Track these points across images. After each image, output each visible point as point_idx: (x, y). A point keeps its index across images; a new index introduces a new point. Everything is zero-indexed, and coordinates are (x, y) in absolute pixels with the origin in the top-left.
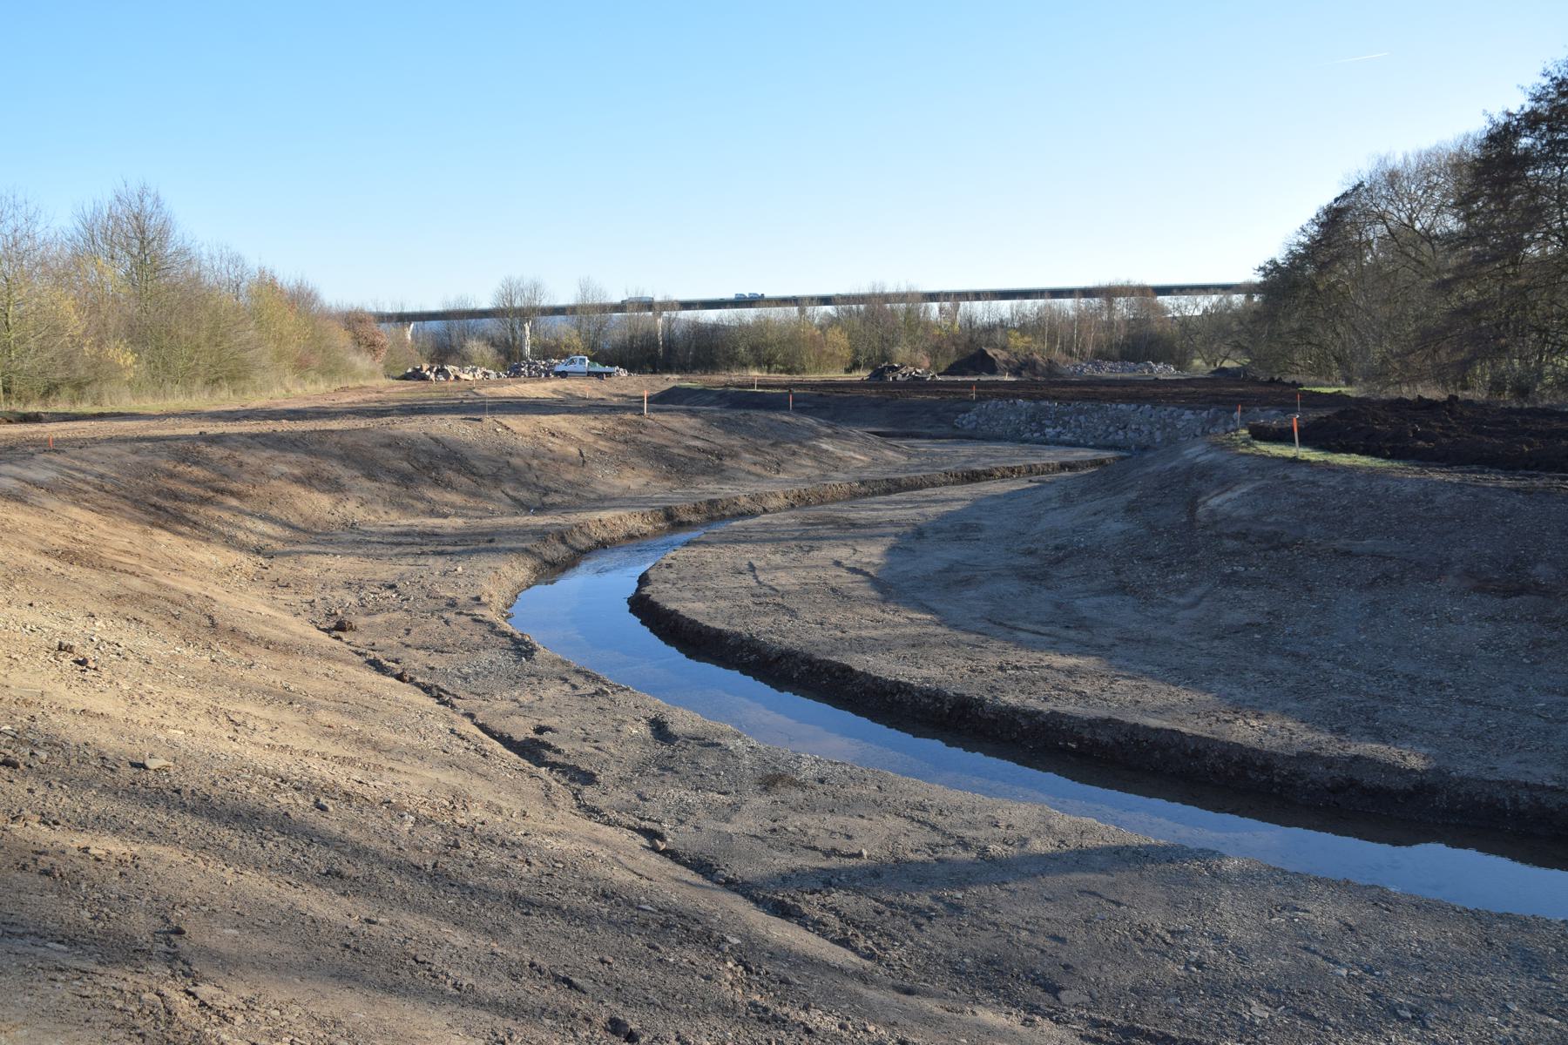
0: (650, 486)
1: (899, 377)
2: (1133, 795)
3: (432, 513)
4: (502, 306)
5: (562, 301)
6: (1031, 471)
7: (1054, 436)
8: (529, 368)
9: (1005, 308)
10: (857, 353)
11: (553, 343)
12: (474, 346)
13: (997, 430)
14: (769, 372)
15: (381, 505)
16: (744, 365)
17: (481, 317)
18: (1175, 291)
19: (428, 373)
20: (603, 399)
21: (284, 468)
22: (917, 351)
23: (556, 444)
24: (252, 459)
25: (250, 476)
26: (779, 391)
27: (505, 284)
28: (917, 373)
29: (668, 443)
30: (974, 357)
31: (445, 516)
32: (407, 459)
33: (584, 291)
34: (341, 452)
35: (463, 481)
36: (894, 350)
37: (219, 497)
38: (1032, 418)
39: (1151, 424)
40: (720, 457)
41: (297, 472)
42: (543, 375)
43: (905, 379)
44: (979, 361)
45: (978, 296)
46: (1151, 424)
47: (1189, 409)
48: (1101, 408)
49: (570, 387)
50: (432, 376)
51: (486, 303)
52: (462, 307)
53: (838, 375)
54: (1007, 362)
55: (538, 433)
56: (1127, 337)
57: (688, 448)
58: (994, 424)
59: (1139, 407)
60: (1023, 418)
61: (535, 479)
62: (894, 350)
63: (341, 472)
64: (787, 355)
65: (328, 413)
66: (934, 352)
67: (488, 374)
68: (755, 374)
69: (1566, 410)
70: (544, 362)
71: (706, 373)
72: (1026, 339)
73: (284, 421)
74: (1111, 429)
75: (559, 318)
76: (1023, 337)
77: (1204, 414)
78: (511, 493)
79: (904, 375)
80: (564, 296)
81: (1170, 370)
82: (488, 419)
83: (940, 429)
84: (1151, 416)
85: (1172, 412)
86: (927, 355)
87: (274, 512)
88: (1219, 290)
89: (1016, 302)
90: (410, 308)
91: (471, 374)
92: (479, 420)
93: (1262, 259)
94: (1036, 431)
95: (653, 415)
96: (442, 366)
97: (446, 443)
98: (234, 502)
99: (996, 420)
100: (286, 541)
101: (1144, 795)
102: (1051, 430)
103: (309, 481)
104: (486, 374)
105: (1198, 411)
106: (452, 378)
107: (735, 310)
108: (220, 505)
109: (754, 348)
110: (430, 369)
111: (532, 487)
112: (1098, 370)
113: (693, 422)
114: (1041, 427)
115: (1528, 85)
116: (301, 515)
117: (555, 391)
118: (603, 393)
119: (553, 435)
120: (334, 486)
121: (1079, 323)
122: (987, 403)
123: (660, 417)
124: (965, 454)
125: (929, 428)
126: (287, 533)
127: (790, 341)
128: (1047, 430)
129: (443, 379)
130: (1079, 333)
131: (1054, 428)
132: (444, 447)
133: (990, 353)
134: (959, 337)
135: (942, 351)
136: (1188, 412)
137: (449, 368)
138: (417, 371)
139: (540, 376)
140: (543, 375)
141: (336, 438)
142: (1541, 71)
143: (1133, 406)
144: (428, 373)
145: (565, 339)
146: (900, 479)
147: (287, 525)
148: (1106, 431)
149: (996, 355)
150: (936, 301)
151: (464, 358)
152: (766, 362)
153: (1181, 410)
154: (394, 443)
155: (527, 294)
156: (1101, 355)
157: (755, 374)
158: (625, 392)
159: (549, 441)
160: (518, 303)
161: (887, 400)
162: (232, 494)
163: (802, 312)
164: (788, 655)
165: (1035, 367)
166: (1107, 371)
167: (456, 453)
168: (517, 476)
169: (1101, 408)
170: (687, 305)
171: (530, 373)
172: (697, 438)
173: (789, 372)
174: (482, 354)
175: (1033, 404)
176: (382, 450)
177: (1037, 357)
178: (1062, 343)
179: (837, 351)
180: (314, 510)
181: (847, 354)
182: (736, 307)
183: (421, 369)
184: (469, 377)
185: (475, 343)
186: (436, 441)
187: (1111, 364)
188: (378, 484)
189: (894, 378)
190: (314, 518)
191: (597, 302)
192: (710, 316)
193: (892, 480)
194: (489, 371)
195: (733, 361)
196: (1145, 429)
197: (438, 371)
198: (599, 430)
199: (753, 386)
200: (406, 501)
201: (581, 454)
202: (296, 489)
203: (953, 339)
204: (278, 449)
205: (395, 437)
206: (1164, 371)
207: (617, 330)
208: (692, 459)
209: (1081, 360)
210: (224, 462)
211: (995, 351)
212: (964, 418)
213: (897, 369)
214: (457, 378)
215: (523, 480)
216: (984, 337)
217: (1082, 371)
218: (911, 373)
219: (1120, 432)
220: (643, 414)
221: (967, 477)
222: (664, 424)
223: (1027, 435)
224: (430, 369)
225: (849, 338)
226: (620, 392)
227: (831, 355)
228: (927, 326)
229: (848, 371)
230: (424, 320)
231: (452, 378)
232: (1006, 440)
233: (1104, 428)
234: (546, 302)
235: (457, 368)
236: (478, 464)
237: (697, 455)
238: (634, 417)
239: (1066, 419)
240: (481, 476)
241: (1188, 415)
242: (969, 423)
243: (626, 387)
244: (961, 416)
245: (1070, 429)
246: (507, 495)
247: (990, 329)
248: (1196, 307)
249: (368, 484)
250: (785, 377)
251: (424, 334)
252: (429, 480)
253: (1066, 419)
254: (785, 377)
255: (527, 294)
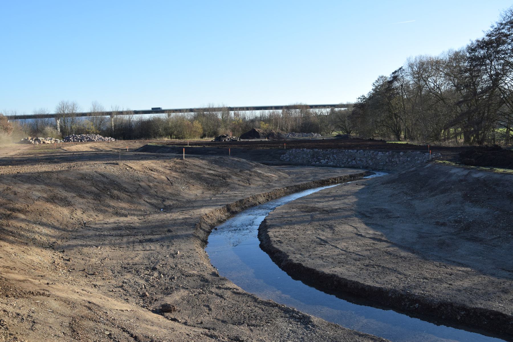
0: (204, 194)
1: (227, 140)
2: (479, 335)
3: (117, 214)
4: (59, 113)
5: (86, 110)
6: (341, 179)
7: (325, 163)
8: (73, 138)
9: (258, 113)
10: (204, 131)
11: (82, 128)
12: (48, 129)
13: (299, 161)
14: (171, 138)
15: (92, 211)
16: (161, 136)
17: (51, 117)
18: (314, 107)
19: (31, 141)
20: (111, 151)
21: (38, 194)
22: (227, 129)
23: (155, 174)
24: (22, 189)
25: (23, 200)
26: (197, 146)
27: (61, 104)
28: (233, 138)
29: (200, 173)
30: (250, 132)
31: (126, 216)
32: (93, 185)
33: (94, 106)
34: (61, 184)
35: (123, 195)
36: (218, 129)
37: (14, 214)
38: (313, 156)
39: (366, 158)
40: (224, 178)
41: (45, 195)
42: (80, 141)
43: (229, 140)
44: (253, 133)
45: (248, 109)
46: (366, 158)
47: (380, 151)
48: (342, 151)
49: (96, 146)
50: (33, 142)
51: (53, 112)
52: (43, 113)
53: (197, 139)
54: (263, 133)
55: (145, 170)
56: (302, 124)
57: (209, 174)
58: (298, 158)
59: (357, 151)
60: (309, 156)
61: (155, 193)
62: (218, 129)
63: (66, 195)
64: (178, 132)
65: (23, 161)
66: (233, 130)
67: (57, 141)
68: (166, 139)
69: (512, 150)
70: (79, 136)
71: (146, 139)
72: (267, 125)
73: (10, 166)
74: (349, 160)
75: (84, 117)
76: (265, 124)
77: (387, 153)
78: (148, 201)
79: (228, 139)
80: (86, 110)
81: (319, 136)
82: (122, 163)
83: (275, 161)
84: (364, 155)
85: (373, 153)
86: (231, 131)
87: (44, 220)
88: (329, 107)
89: (261, 111)
90: (19, 113)
91: (50, 141)
92: (117, 164)
93: (360, 95)
94: (316, 161)
95: (186, 159)
96: (37, 138)
97: (108, 177)
98: (22, 216)
99: (298, 157)
100: (58, 238)
101: (469, 331)
102: (323, 161)
103: (53, 199)
104: (56, 141)
105: (384, 152)
106: (42, 143)
107: (157, 114)
108: (16, 218)
109: (165, 129)
110: (32, 139)
111: (156, 197)
112: (294, 136)
113: (204, 162)
114: (319, 160)
115: (485, 30)
116: (58, 221)
117: (91, 148)
118: (110, 148)
119: (152, 170)
120: (66, 203)
121: (285, 118)
122: (292, 150)
123: (191, 160)
124: (322, 174)
125: (270, 161)
126: (57, 233)
127: (179, 126)
128: (321, 161)
129: (37, 143)
130: (285, 122)
131: (324, 160)
132: (107, 178)
133: (256, 130)
134: (242, 124)
135: (236, 130)
136: (380, 153)
137: (40, 138)
138: (26, 139)
139: (78, 141)
140: (80, 141)
141: (55, 176)
142: (490, 25)
143: (355, 151)
144: (31, 141)
145: (87, 126)
146: (299, 185)
147: (54, 227)
148: (347, 161)
149: (259, 131)
150: (232, 111)
151: (44, 134)
152: (170, 134)
153: (377, 152)
154: (83, 177)
155: (70, 108)
156: (293, 131)
157: (166, 139)
158: (119, 147)
159: (152, 173)
160: (66, 112)
161: (248, 149)
162: (20, 211)
163: (169, 116)
164: (443, 305)
165: (273, 135)
166: (298, 136)
167: (114, 181)
168: (146, 191)
169: (342, 151)
170: (136, 112)
171: (74, 140)
172: (210, 169)
173: (179, 138)
174: (52, 132)
175: (311, 150)
176: (80, 181)
177: (274, 131)
178: (279, 126)
179: (197, 130)
180: (63, 218)
181: (201, 131)
182: (156, 113)
183: (28, 139)
184: (49, 142)
185: (49, 128)
186: (103, 175)
187: (298, 134)
188: (86, 200)
189: (225, 140)
190: (65, 223)
191: (100, 111)
192: (147, 117)
193: (296, 186)
194: (57, 140)
195: (157, 134)
196: (364, 159)
197: (35, 140)
198: (169, 167)
199: (187, 145)
200: (103, 208)
201: (168, 179)
202: (49, 206)
203: (240, 124)
204: (30, 183)
205: (83, 174)
206: (318, 136)
207: (110, 122)
208: (214, 180)
209: (287, 132)
210: (6, 192)
211: (259, 129)
212: (284, 157)
213: (225, 137)
214: (44, 142)
215: (150, 194)
216: (251, 124)
217: (288, 136)
218: (231, 138)
219: (354, 161)
220: (183, 159)
221: (321, 183)
222: (194, 163)
223: (314, 163)
224: (32, 139)
225: (202, 125)
226: (117, 148)
227: (195, 131)
228: (231, 120)
229: (202, 138)
230: (25, 119)
231: (42, 143)
232: (305, 165)
233: (346, 160)
234: (79, 111)
235: (43, 139)
236: (125, 186)
237: (215, 178)
238: (180, 161)
239: (328, 156)
240: (131, 193)
241: (380, 154)
242: (287, 158)
243: (119, 145)
244: (282, 156)
245: (331, 160)
246: (147, 202)
247: (252, 121)
248: (326, 111)
249: (81, 200)
250: (177, 141)
251: (249, 119)
252: (108, 196)
253: (328, 156)
254: (177, 141)
255: (70, 108)
